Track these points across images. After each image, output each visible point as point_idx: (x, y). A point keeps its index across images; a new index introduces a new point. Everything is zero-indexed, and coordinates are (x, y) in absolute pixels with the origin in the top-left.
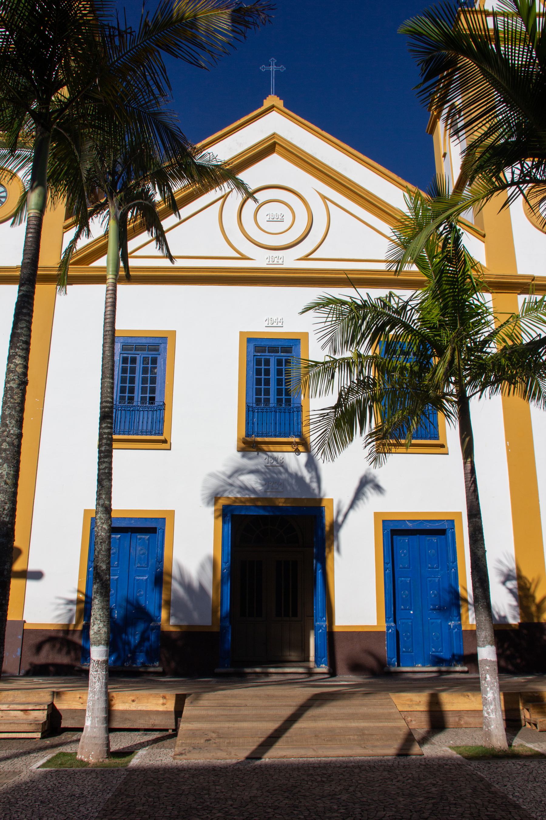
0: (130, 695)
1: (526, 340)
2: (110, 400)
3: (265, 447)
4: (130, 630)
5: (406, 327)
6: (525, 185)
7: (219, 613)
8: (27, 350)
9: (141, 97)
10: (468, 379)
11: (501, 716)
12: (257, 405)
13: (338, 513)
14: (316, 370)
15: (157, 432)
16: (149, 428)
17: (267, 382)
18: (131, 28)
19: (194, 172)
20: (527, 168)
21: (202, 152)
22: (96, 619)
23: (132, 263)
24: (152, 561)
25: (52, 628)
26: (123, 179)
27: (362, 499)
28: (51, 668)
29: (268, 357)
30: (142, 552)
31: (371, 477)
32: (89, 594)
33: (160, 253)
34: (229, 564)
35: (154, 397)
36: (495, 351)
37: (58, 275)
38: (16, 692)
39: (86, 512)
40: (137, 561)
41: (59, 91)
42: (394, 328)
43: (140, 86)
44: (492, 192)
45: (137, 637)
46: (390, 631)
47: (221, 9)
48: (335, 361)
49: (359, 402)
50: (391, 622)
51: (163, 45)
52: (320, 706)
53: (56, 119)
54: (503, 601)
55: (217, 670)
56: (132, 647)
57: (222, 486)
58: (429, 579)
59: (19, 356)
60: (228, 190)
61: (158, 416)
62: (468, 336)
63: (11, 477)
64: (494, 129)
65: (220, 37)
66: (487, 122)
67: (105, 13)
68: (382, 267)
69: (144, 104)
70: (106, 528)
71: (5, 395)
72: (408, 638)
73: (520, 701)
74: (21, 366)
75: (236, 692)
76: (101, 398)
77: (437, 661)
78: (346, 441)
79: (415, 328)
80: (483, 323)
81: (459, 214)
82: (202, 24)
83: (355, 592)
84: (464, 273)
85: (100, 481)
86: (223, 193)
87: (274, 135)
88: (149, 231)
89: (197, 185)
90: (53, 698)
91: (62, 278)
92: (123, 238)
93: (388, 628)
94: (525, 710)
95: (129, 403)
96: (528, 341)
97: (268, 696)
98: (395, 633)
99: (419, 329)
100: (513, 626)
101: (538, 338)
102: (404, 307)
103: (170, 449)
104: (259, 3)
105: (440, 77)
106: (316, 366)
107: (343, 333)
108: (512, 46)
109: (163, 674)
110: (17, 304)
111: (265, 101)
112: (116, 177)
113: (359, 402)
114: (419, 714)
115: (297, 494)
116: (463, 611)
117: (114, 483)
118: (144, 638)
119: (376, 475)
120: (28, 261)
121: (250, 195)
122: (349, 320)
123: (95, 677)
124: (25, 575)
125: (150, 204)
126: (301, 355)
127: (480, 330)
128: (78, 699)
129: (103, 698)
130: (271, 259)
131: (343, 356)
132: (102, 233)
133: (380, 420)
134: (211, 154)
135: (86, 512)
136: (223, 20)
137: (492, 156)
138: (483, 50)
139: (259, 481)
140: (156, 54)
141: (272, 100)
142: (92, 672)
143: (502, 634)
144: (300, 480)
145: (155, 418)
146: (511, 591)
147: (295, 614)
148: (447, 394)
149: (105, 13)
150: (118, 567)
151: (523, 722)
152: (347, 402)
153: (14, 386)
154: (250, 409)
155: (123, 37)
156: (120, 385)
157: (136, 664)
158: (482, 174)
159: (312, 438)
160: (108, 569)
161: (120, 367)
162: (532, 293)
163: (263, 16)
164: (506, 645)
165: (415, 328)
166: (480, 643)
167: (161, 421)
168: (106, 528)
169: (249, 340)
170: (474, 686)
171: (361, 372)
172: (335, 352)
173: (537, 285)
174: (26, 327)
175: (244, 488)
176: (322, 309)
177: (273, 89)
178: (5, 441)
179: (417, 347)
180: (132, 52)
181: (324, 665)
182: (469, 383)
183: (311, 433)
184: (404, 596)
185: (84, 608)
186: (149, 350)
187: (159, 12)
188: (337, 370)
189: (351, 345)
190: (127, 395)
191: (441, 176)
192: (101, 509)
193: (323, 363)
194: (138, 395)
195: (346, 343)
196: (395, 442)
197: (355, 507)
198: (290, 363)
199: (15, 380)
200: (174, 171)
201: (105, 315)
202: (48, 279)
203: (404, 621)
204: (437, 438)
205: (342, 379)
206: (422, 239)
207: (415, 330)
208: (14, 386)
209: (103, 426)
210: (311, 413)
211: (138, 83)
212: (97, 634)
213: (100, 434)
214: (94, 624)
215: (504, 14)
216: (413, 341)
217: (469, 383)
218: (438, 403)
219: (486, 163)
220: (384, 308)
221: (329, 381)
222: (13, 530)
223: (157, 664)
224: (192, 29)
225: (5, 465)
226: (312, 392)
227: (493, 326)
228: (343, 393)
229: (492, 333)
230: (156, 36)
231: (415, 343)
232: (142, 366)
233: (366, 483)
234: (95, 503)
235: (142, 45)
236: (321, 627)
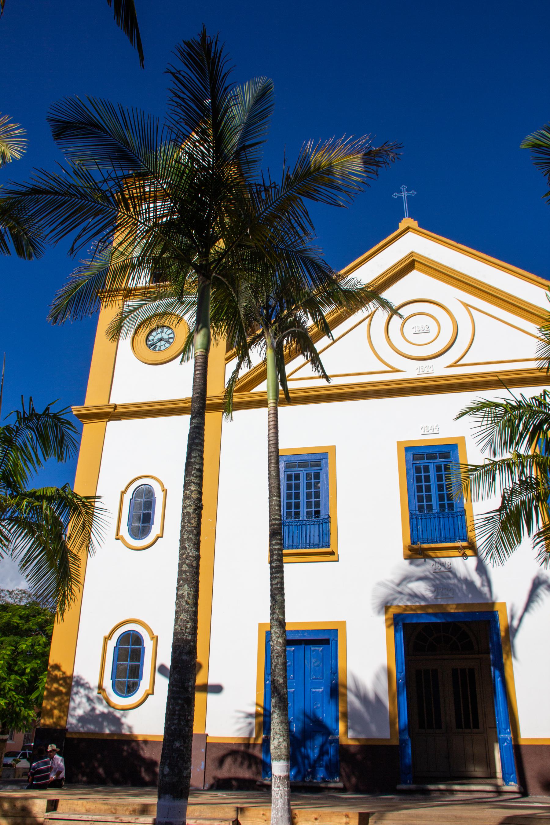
0: (313, 813)
2: (278, 517)
3: (431, 553)
4: (308, 743)
7: (397, 725)
8: (201, 477)
12: (420, 512)
13: (512, 617)
14: (477, 473)
15: (324, 544)
16: (316, 541)
17: (428, 489)
18: (275, 183)
19: (343, 299)
22: (276, 733)
23: (291, 385)
24: (327, 673)
25: (233, 742)
26: (277, 312)
27: (537, 602)
28: (234, 783)
30: (316, 664)
31: (543, 578)
32: (267, 707)
34: (404, 673)
35: (319, 511)
37: (224, 403)
38: (203, 807)
39: (261, 625)
40: (312, 675)
41: (216, 244)
45: (317, 751)
48: (495, 463)
49: (523, 502)
51: (303, 192)
53: (214, 268)
55: (399, 787)
56: (312, 761)
57: (392, 595)
59: (194, 483)
60: (373, 310)
61: (324, 529)
63: (191, 597)
65: (355, 178)
67: (252, 174)
68: (534, 365)
69: (290, 244)
70: (282, 642)
71: (183, 520)
74: (196, 492)
75: (421, 811)
76: (270, 516)
78: (515, 544)
82: (337, 171)
85: (273, 596)
86: (370, 312)
88: (304, 355)
90: (238, 814)
91: (228, 406)
92: (280, 363)
95: (295, 518)
97: (456, 817)
103: (338, 561)
104: (387, 144)
106: (476, 469)
107: (501, 435)
109: (343, 790)
110: (189, 435)
112: (270, 311)
113: (523, 502)
115: (470, 599)
117: (286, 597)
118: (323, 752)
120: (197, 395)
121: (395, 312)
123: (277, 794)
124: (206, 688)
125: (303, 331)
128: (261, 815)
129: (286, 816)
130: (421, 369)
132: (261, 360)
134: (355, 279)
135: (261, 625)
136: (356, 164)
139: (429, 588)
140: (298, 200)
141: (407, 222)
142: (274, 788)
144: (470, 584)
145: (321, 531)
147: (476, 726)
149: (252, 174)
150: (294, 679)
152: (511, 504)
153: (191, 511)
154: (414, 516)
155: (268, 191)
156: (286, 501)
157: (316, 779)
160: (285, 682)
161: (285, 484)
163: (391, 155)
167: (328, 534)
168: (282, 642)
171: (522, 472)
172: (495, 454)
174: (199, 456)
175: (414, 596)
176: (477, 413)
177: (406, 212)
178: (185, 563)
180: (277, 202)
181: (513, 783)
183: (477, 538)
185: (264, 722)
186: (312, 466)
187: (298, 165)
188: (497, 472)
190: (293, 510)
192: (275, 623)
194: (303, 510)
197: (530, 610)
198: (449, 468)
199: (191, 506)
201: (269, 438)
202: (216, 407)
205: (504, 481)
208: (191, 511)
209: (274, 542)
210: (475, 518)
211: (284, 227)
212: (277, 749)
213: (271, 551)
214: (274, 738)
220: (539, 407)
222: (195, 648)
223: (337, 779)
224: (328, 175)
225: (186, 586)
226: (474, 495)
228: (506, 495)
230: (297, 186)
232: (305, 481)
234: (269, 617)
236: (505, 740)
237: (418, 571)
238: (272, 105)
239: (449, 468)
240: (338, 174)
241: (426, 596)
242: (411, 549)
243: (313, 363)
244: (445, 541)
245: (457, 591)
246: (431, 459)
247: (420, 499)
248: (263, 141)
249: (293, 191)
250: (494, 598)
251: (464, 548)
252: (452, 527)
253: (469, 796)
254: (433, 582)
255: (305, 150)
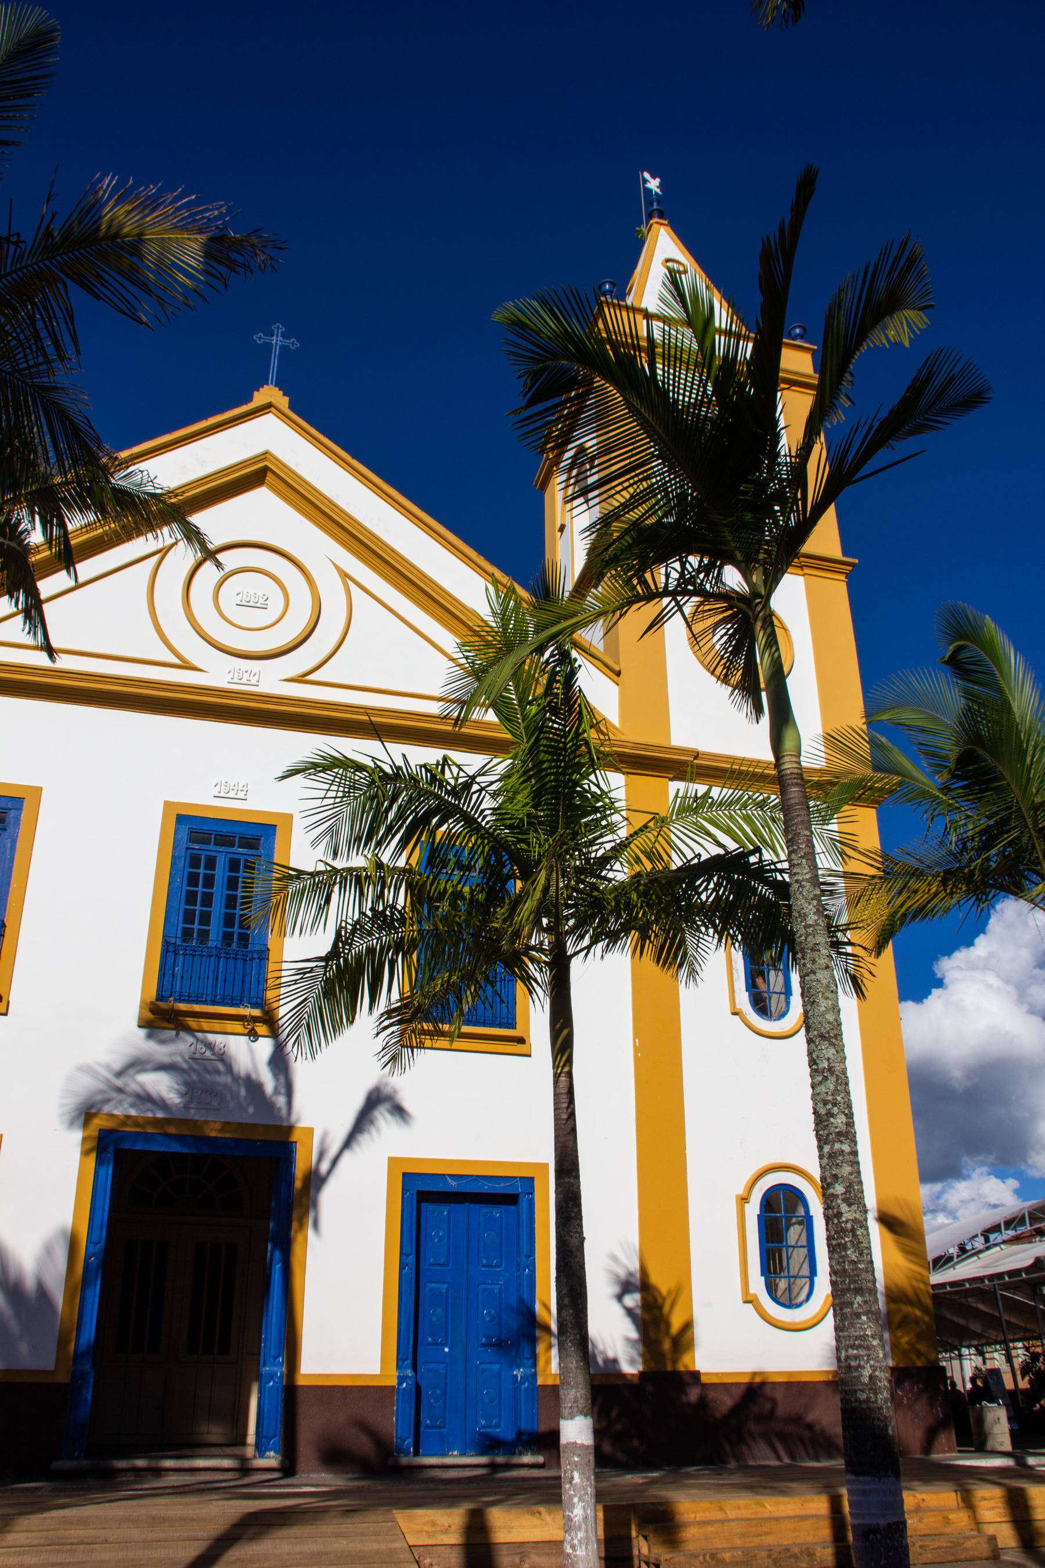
1: (677, 862)
3: (192, 1022)
5: (469, 821)
6: (686, 598)
9: (22, 355)
10: (571, 922)
11: (596, 1552)
12: (184, 941)
17: (208, 900)
18: (18, 235)
20: (691, 570)
21: (128, 467)
27: (369, 1132)
29: (213, 854)
31: (388, 1090)
33: (29, 640)
36: (621, 877)
42: (447, 821)
43: (22, 337)
44: (630, 603)
46: (404, 1385)
47: (189, 231)
48: (335, 871)
49: (371, 951)
50: (407, 1368)
52: (255, 1538)
54: (611, 1330)
55: (56, 1465)
57: (102, 1092)
58: (483, 1286)
60: (169, 541)
62: (577, 847)
64: (641, 498)
65: (182, 278)
66: (631, 485)
68: (434, 708)
72: (437, 1399)
73: (633, 1521)
77: (489, 1444)
79: (483, 824)
80: (605, 827)
81: (573, 633)
82: (151, 252)
83: (343, 1310)
84: (577, 734)
86: (160, 546)
87: (265, 455)
88: (12, 597)
89: (113, 525)
93: (401, 1379)
94: (641, 1538)
96: (680, 863)
97: (154, 1518)
98: (414, 1390)
99: (490, 827)
100: (629, 1377)
101: (696, 861)
102: (467, 786)
103: (6, 1014)
105: (564, 397)
106: (298, 877)
107: (353, 821)
108: (675, 371)
111: (256, 393)
114: (448, 1550)
115: (250, 1114)
116: (540, 1348)
119: (397, 1087)
121: (210, 555)
122: (367, 800)
125: (18, 548)
126: (276, 855)
127: (596, 839)
131: (349, 865)
133: (407, 988)
134: (145, 473)
136: (190, 251)
137: (636, 542)
138: (627, 368)
139: (176, 1086)
140: (60, 286)
141: (269, 394)
143: (606, 1392)
144: (254, 1086)
146: (630, 1312)
148: (533, 948)
151: (636, 1561)
152: (350, 950)
154: (171, 948)
158: (616, 570)
159: (282, 1011)
162: (691, 780)
164: (614, 1414)
165: (483, 824)
166: (565, 1412)
169: (181, 819)
170: (549, 1493)
173: (699, 767)
175: (145, 1098)
177: (273, 374)
179: (485, 859)
181: (272, 1453)
182: (572, 931)
183: (282, 1002)
184: (434, 1319)
188: (337, 888)
189: (366, 845)
191: (554, 564)
193: (312, 875)
195: (357, 841)
196: (431, 1028)
198: (253, 869)
200: (71, 494)
203: (431, 1366)
204: (512, 1025)
205: (344, 907)
206: (507, 667)
207: (484, 828)
211: (19, 331)
215: (665, 319)
216: (479, 847)
217: (572, 931)
218: (514, 962)
219: (626, 553)
221: (320, 908)
224: (131, 255)
227: (623, 833)
229: (619, 845)
230: (65, 257)
231: (482, 852)
233: (377, 1102)
235: (35, 267)
236: (272, 1376)
237: (161, 1052)
238: (47, 76)
239: (253, 869)
240: (150, 260)
241: (169, 1102)
242: (154, 1009)
243: (28, 617)
244: (223, 1003)
245: (229, 1098)
246: (221, 845)
247: (189, 917)
248: (13, 144)
249: (52, 264)
250: (293, 1118)
251: (255, 1020)
252: (239, 978)
253: (188, 1478)
254: (186, 1077)
255: (97, 192)
